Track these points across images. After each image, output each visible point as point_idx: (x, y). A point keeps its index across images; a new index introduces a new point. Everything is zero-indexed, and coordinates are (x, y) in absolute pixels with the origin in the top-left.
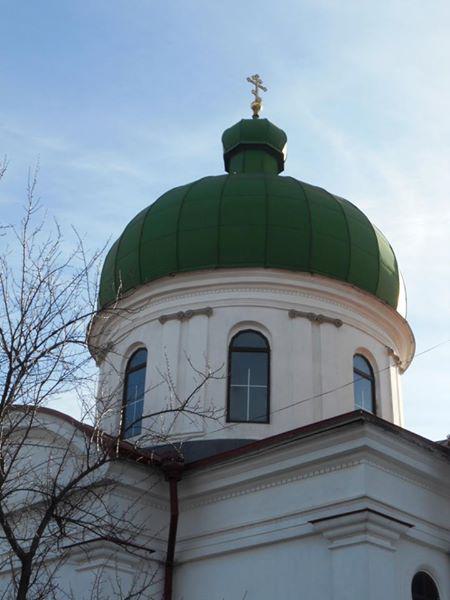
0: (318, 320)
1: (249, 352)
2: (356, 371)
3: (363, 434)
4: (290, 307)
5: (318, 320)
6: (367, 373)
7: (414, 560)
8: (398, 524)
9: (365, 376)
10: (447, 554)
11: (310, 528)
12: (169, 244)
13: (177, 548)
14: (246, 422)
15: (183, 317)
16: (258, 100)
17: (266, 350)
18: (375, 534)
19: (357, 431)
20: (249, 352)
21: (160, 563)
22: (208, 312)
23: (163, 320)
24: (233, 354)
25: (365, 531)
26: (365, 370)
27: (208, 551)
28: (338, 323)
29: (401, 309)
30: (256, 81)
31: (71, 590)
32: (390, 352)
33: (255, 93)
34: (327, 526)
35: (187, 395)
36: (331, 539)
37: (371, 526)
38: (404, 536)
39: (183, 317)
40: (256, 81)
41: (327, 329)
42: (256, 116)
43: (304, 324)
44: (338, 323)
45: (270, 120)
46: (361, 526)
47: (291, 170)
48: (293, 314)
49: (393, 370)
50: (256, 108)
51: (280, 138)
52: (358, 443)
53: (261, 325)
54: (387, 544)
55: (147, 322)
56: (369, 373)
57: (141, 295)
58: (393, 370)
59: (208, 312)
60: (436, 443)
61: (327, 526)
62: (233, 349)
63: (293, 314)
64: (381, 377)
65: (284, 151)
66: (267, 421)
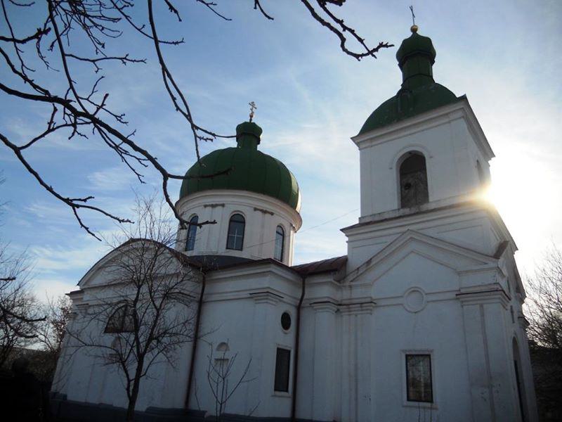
0: (265, 212)
1: (237, 222)
2: (277, 232)
3: (270, 267)
4: (254, 206)
5: (265, 212)
6: (282, 234)
7: (284, 308)
8: (278, 297)
9: (281, 234)
10: (296, 307)
11: (249, 296)
12: (211, 175)
13: (204, 297)
14: (243, 238)
15: (213, 206)
16: (253, 113)
17: (243, 222)
18: (270, 300)
19: (269, 266)
20: (237, 222)
21: (197, 302)
22: (223, 205)
23: (206, 206)
24: (232, 223)
25: (267, 299)
26: (280, 231)
27: (213, 299)
28: (272, 214)
29: (298, 209)
30: (252, 104)
31: (372, 303)
32: (292, 225)
33: (252, 110)
34: (256, 296)
35: (211, 241)
36: (256, 300)
37: (269, 301)
38: (281, 301)
39: (213, 206)
40: (252, 104)
41: (268, 216)
42: (251, 120)
43: (260, 213)
44: (272, 214)
45: (240, 123)
46: (265, 301)
47: (260, 148)
48: (255, 209)
49: (292, 232)
50: (251, 116)
51: (259, 131)
52: (268, 269)
53: (241, 212)
54: (274, 303)
55: (199, 206)
56: (282, 233)
57: (197, 195)
58: (292, 232)
59: (223, 205)
60: (404, 80)
61: (256, 296)
62: (231, 221)
63: (255, 209)
64: (286, 234)
65: (261, 137)
66: (241, 250)
